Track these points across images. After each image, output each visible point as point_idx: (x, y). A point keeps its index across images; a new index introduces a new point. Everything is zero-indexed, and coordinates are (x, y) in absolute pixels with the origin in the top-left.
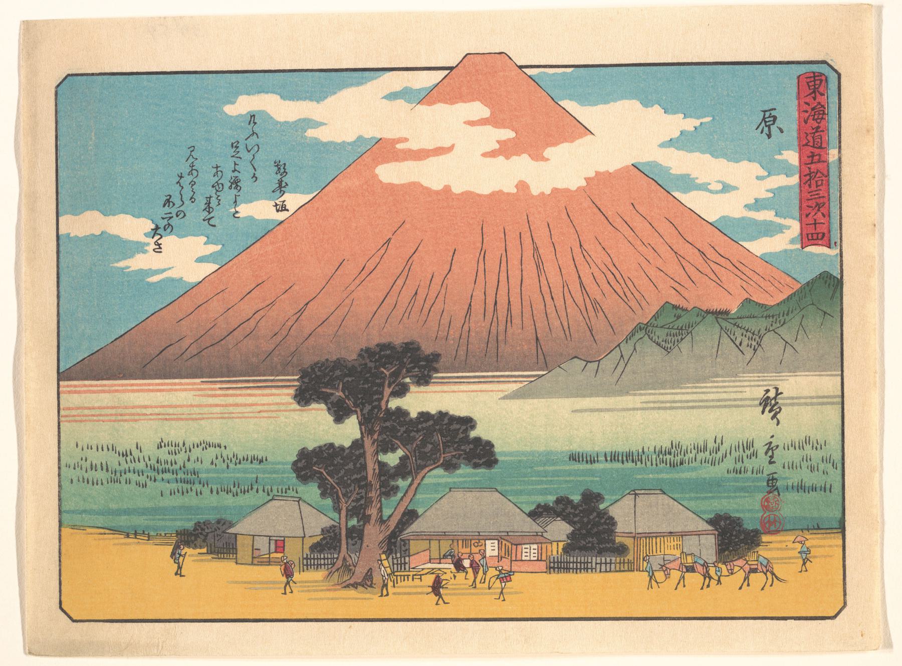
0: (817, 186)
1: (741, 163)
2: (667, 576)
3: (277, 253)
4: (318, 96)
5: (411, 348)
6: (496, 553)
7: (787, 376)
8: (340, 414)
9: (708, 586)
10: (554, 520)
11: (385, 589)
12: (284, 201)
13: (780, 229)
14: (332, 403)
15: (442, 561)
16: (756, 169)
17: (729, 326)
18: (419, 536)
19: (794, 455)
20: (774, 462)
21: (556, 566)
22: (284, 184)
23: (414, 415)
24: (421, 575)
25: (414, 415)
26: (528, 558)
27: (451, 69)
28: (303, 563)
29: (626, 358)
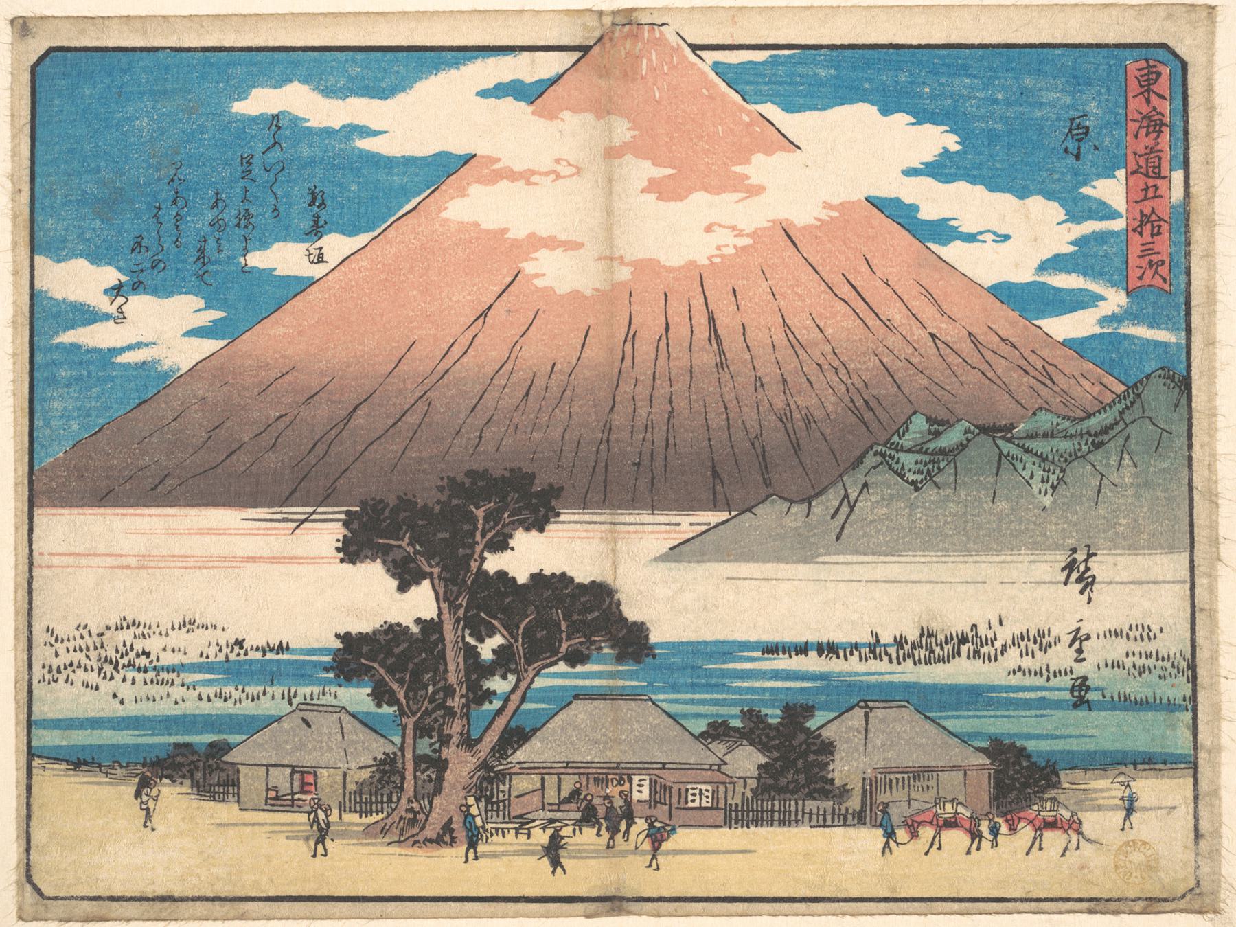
0: (1152, 235)
2: (914, 835)
8: (406, 577)
10: (741, 745)
11: (472, 851)
13: (1093, 300)
14: (394, 561)
15: (562, 808)
16: (1054, 211)
17: (1014, 450)
18: (526, 769)
19: (1117, 650)
22: (321, 223)
23: (522, 579)
24: (529, 829)
25: (522, 579)
26: (696, 804)
27: (585, 50)
28: (355, 800)
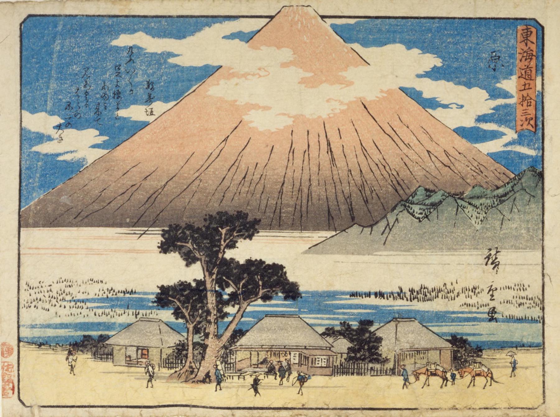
1: (439, 82)
2: (417, 378)
3: (510, 114)
4: (180, 35)
5: (241, 216)
6: (297, 361)
7: (462, 313)
8: (190, 259)
9: (446, 386)
12: (152, 109)
20: (494, 300)
21: (342, 370)
26: (320, 365)
27: (272, 17)
29: (391, 225)
